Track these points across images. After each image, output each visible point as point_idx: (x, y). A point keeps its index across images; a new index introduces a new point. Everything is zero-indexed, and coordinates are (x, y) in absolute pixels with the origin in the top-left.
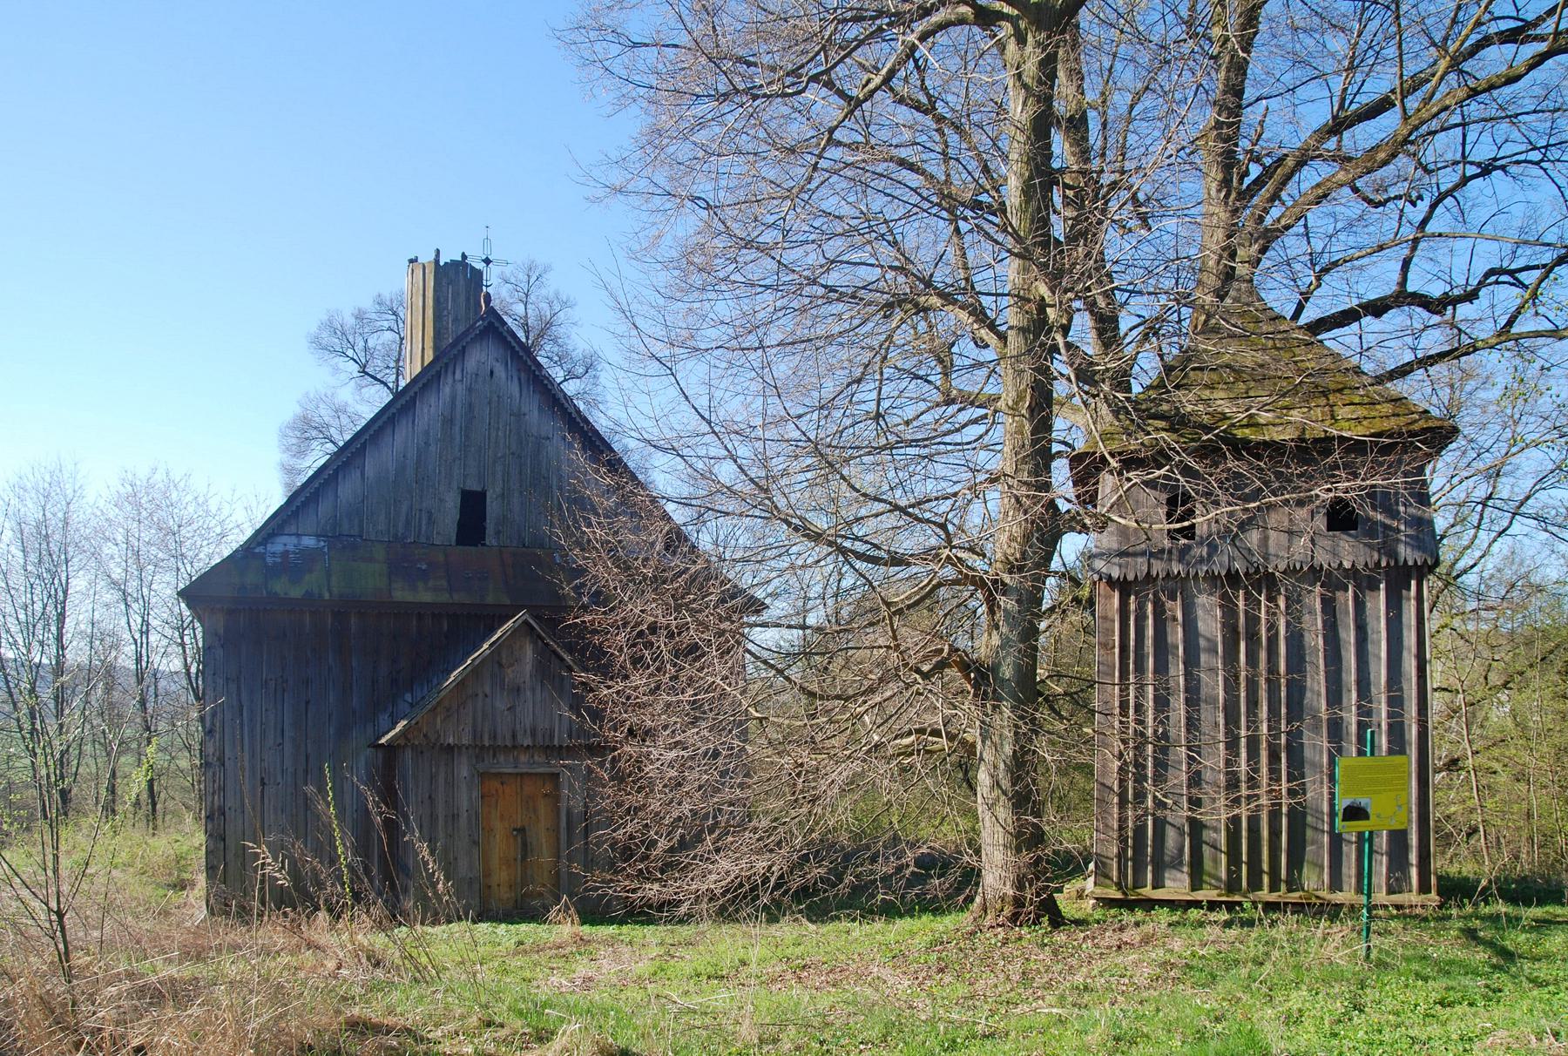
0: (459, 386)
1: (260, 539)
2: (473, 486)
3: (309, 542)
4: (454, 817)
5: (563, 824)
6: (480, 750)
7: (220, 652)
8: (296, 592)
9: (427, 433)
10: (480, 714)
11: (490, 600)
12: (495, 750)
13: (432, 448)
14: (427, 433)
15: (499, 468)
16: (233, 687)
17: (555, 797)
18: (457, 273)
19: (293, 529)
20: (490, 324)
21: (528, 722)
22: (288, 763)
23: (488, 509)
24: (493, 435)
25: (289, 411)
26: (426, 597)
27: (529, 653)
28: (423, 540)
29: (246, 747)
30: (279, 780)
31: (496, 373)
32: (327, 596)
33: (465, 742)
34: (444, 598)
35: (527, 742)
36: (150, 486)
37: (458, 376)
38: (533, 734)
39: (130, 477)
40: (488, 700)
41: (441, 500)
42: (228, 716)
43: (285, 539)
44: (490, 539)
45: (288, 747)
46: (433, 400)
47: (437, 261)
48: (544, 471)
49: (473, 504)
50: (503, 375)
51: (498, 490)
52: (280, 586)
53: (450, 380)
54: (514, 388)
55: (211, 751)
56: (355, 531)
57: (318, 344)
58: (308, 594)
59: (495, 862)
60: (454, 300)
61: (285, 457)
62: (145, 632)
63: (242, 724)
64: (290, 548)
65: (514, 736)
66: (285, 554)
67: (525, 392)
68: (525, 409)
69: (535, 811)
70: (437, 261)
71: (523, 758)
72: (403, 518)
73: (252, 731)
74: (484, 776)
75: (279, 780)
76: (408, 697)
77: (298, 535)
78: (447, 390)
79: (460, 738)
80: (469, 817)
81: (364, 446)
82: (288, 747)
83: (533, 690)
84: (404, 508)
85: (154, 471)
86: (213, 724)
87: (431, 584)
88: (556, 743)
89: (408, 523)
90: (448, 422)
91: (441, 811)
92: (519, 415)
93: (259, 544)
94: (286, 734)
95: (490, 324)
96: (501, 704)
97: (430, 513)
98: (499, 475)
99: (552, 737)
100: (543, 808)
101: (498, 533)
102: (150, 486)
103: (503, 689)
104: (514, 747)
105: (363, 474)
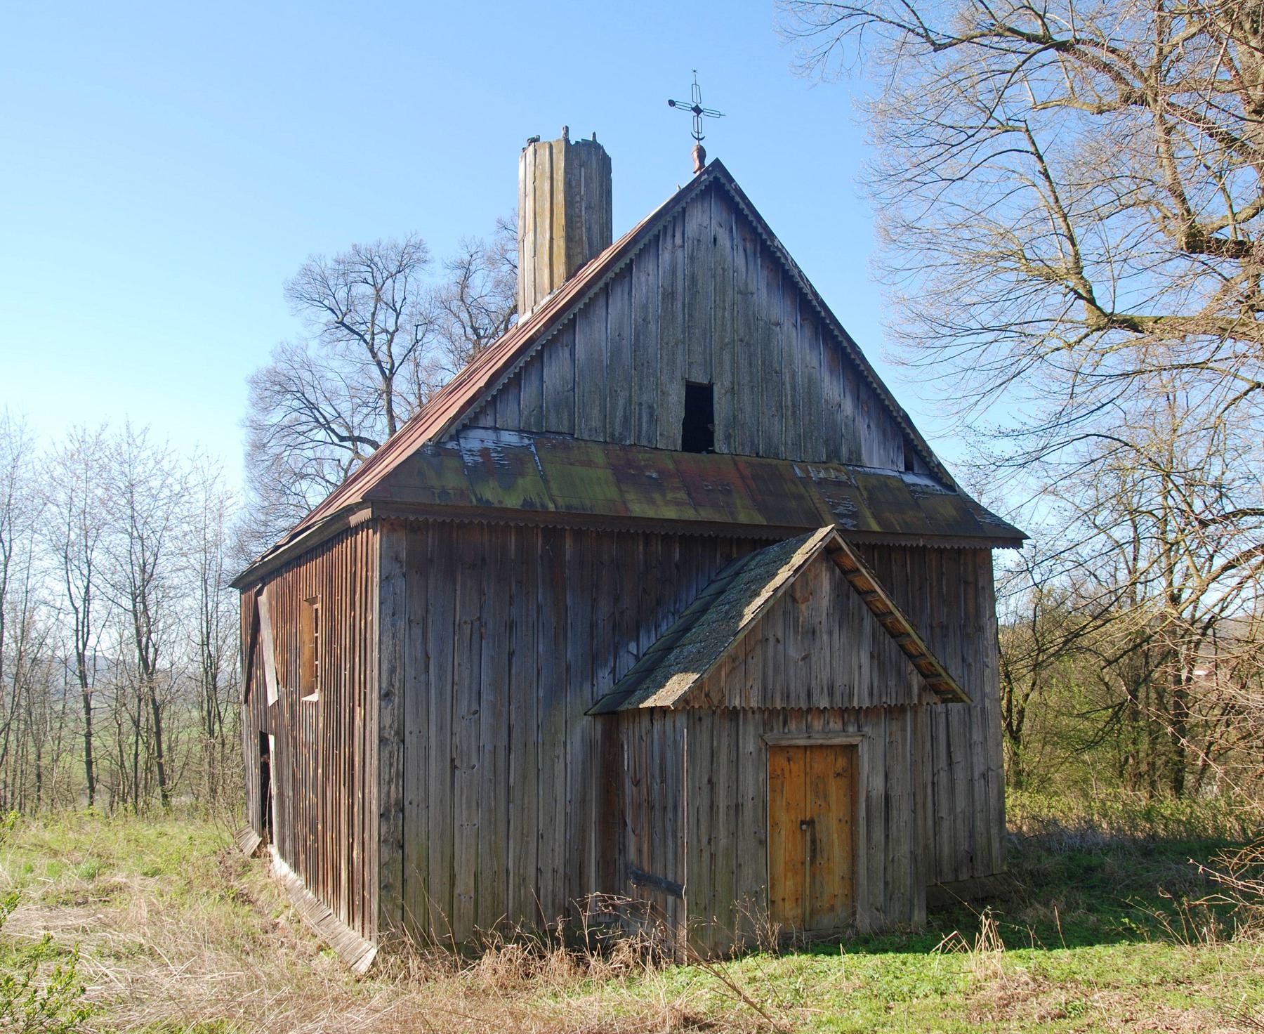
0: (679, 253)
1: (453, 430)
2: (700, 378)
3: (510, 438)
4: (738, 808)
5: (862, 813)
6: (771, 716)
7: (400, 585)
8: (513, 501)
9: (645, 307)
10: (771, 665)
11: (743, 518)
12: (786, 715)
13: (652, 327)
14: (645, 307)
15: (727, 357)
16: (417, 631)
17: (851, 777)
18: (589, 154)
19: (489, 421)
20: (716, 179)
21: (824, 676)
22: (486, 739)
23: (716, 406)
24: (720, 314)
25: (263, 361)
26: (670, 513)
27: (825, 583)
28: (644, 442)
29: (433, 717)
30: (474, 761)
31: (720, 241)
32: (551, 507)
33: (754, 704)
34: (689, 514)
35: (824, 703)
36: (98, 443)
37: (678, 241)
38: (831, 694)
39: (80, 433)
40: (780, 647)
41: (663, 393)
42: (411, 673)
43: (479, 433)
44: (720, 446)
45: (486, 716)
46: (651, 267)
47: (567, 141)
48: (776, 365)
49: (699, 400)
50: (728, 244)
51: (727, 384)
52: (490, 492)
53: (669, 245)
54: (740, 261)
55: (387, 722)
56: (564, 429)
57: (295, 294)
58: (527, 503)
59: (780, 867)
60: (587, 185)
61: (252, 412)
62: (87, 600)
63: (428, 684)
64: (490, 445)
65: (809, 695)
66: (485, 452)
67: (751, 267)
68: (752, 288)
69: (826, 797)
70: (567, 141)
71: (818, 725)
72: (620, 413)
73: (441, 693)
74: (776, 749)
75: (474, 761)
76: (632, 647)
77: (495, 429)
78: (666, 256)
79: (748, 699)
80: (755, 807)
81: (573, 323)
82: (486, 716)
83: (830, 633)
84: (621, 402)
85: (104, 427)
86: (391, 684)
87: (670, 496)
88: (855, 704)
89: (626, 420)
90: (669, 296)
91: (722, 802)
92: (746, 294)
93: (452, 438)
94: (484, 697)
95: (716, 179)
96: (794, 653)
97: (651, 407)
98: (727, 367)
99: (851, 696)
100: (836, 790)
101: (728, 437)
102: (98, 443)
103: (796, 632)
104: (809, 710)
105: (572, 354)
